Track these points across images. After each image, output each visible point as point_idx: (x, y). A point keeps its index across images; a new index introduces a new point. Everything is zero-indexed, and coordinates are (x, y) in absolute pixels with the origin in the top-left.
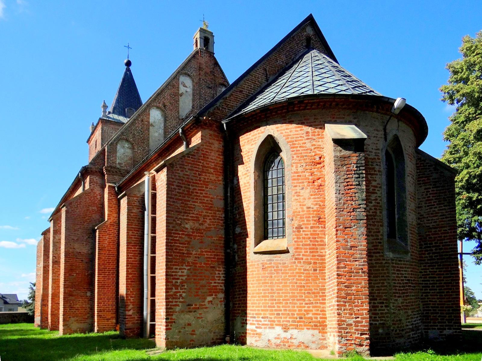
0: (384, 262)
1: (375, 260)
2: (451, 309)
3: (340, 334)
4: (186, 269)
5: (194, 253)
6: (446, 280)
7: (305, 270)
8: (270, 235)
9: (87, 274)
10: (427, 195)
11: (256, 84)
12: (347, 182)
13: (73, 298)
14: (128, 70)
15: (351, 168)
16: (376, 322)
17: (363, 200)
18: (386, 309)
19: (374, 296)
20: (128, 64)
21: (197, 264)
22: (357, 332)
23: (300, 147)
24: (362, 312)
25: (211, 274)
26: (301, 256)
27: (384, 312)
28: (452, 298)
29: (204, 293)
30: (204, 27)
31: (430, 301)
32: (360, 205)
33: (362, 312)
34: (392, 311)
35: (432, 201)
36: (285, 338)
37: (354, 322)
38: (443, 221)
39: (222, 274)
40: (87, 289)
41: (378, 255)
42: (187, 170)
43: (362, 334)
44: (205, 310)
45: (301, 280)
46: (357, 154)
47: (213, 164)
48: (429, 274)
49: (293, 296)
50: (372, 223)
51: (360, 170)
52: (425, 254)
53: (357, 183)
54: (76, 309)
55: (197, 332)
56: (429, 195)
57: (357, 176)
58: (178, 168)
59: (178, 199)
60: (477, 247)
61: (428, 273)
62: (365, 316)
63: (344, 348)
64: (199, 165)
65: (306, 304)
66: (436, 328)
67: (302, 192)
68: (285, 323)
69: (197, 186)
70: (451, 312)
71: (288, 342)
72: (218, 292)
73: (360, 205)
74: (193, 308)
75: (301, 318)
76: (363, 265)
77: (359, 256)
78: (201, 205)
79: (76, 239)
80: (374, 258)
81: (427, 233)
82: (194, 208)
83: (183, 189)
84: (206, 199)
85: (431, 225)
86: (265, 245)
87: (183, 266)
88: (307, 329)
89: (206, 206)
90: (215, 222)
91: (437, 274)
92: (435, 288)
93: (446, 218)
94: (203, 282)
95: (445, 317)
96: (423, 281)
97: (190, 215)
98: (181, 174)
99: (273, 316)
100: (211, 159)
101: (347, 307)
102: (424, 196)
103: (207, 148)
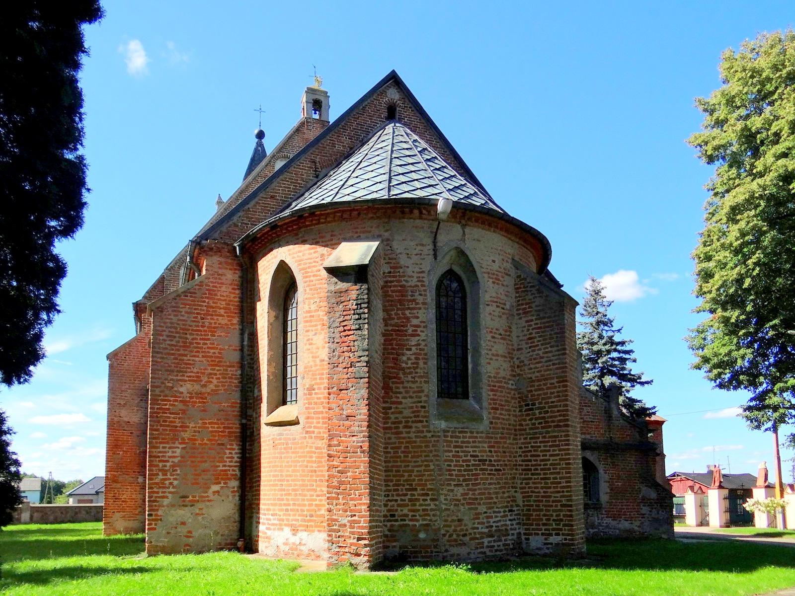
0: (429, 435)
1: (414, 432)
2: (559, 504)
3: (330, 538)
4: (178, 448)
5: (191, 425)
6: (553, 460)
7: (317, 448)
8: (289, 399)
9: (138, 452)
10: (528, 330)
11: (299, 183)
12: (344, 326)
13: (118, 485)
14: (260, 145)
15: (350, 306)
16: (415, 523)
17: (364, 350)
18: (432, 503)
19: (411, 485)
20: (261, 135)
21: (195, 440)
22: (352, 536)
23: (314, 276)
24: (359, 507)
25: (218, 453)
26: (312, 429)
27: (429, 508)
28: (561, 487)
29: (206, 480)
30: (315, 86)
31: (532, 492)
32: (361, 357)
33: (359, 507)
34: (444, 507)
35: (536, 340)
36: (294, 544)
37: (349, 521)
38: (548, 370)
39: (236, 453)
40: (139, 472)
41: (420, 425)
42: (183, 313)
43: (359, 539)
44: (208, 503)
45: (312, 462)
46: (358, 287)
47: (224, 303)
48: (530, 451)
49: (303, 485)
50: (410, 379)
51: (361, 308)
52: (525, 420)
53: (357, 326)
54: (123, 501)
55: (194, 534)
56: (531, 331)
57: (357, 316)
58: (170, 312)
59: (169, 354)
60: (751, 400)
61: (530, 449)
62: (363, 513)
63: (335, 557)
64: (202, 306)
65: (318, 496)
66: (540, 532)
67: (315, 338)
68: (294, 522)
69: (197, 335)
70: (559, 508)
71: (296, 549)
72: (230, 479)
73: (361, 357)
74: (190, 501)
75: (311, 516)
76: (363, 442)
77: (357, 428)
78: (203, 359)
79: (122, 403)
80: (414, 430)
81: (529, 389)
82: (193, 364)
83: (177, 339)
84: (212, 351)
85: (533, 376)
86: (282, 413)
87: (174, 443)
88: (319, 531)
89: (212, 361)
90: (226, 382)
91: (541, 451)
92: (539, 472)
93: (554, 364)
94: (205, 466)
95: (552, 515)
96: (523, 461)
97: (186, 375)
98: (175, 319)
99: (281, 513)
100: (221, 296)
101: (340, 501)
102: (525, 332)
103: (214, 281)
